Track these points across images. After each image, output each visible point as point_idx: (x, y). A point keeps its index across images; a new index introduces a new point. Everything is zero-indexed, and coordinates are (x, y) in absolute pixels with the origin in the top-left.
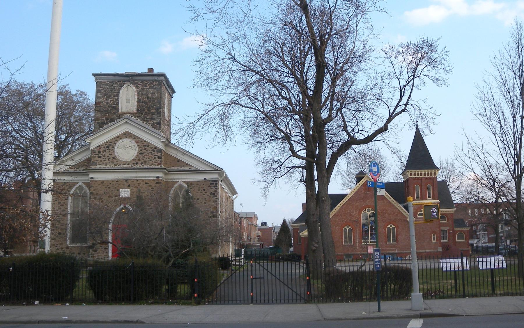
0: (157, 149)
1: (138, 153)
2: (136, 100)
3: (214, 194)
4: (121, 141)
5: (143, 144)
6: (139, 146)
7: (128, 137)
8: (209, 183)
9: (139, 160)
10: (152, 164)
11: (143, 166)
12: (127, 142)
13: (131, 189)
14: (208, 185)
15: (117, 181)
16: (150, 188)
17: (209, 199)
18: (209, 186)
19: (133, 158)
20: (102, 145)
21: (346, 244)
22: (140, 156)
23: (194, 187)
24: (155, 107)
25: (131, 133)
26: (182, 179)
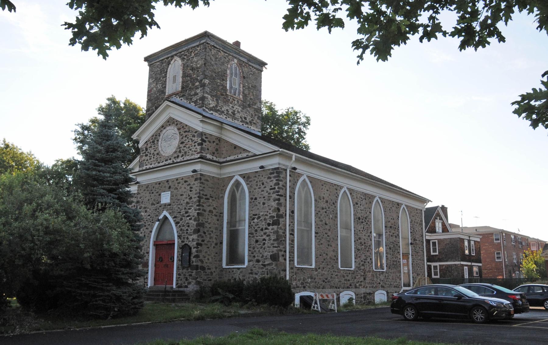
0: (198, 132)
1: (179, 143)
2: (181, 75)
3: (274, 188)
4: (164, 131)
5: (184, 130)
6: (181, 134)
7: (171, 124)
8: (269, 172)
9: (180, 152)
10: (192, 155)
11: (184, 158)
12: (172, 130)
13: (171, 192)
14: (267, 176)
15: (159, 184)
16: (188, 188)
17: (269, 197)
18: (269, 178)
19: (174, 150)
20: (149, 140)
21: (314, 309)
22: (181, 145)
23: (251, 181)
24: (198, 78)
25: (174, 119)
26: (237, 171)
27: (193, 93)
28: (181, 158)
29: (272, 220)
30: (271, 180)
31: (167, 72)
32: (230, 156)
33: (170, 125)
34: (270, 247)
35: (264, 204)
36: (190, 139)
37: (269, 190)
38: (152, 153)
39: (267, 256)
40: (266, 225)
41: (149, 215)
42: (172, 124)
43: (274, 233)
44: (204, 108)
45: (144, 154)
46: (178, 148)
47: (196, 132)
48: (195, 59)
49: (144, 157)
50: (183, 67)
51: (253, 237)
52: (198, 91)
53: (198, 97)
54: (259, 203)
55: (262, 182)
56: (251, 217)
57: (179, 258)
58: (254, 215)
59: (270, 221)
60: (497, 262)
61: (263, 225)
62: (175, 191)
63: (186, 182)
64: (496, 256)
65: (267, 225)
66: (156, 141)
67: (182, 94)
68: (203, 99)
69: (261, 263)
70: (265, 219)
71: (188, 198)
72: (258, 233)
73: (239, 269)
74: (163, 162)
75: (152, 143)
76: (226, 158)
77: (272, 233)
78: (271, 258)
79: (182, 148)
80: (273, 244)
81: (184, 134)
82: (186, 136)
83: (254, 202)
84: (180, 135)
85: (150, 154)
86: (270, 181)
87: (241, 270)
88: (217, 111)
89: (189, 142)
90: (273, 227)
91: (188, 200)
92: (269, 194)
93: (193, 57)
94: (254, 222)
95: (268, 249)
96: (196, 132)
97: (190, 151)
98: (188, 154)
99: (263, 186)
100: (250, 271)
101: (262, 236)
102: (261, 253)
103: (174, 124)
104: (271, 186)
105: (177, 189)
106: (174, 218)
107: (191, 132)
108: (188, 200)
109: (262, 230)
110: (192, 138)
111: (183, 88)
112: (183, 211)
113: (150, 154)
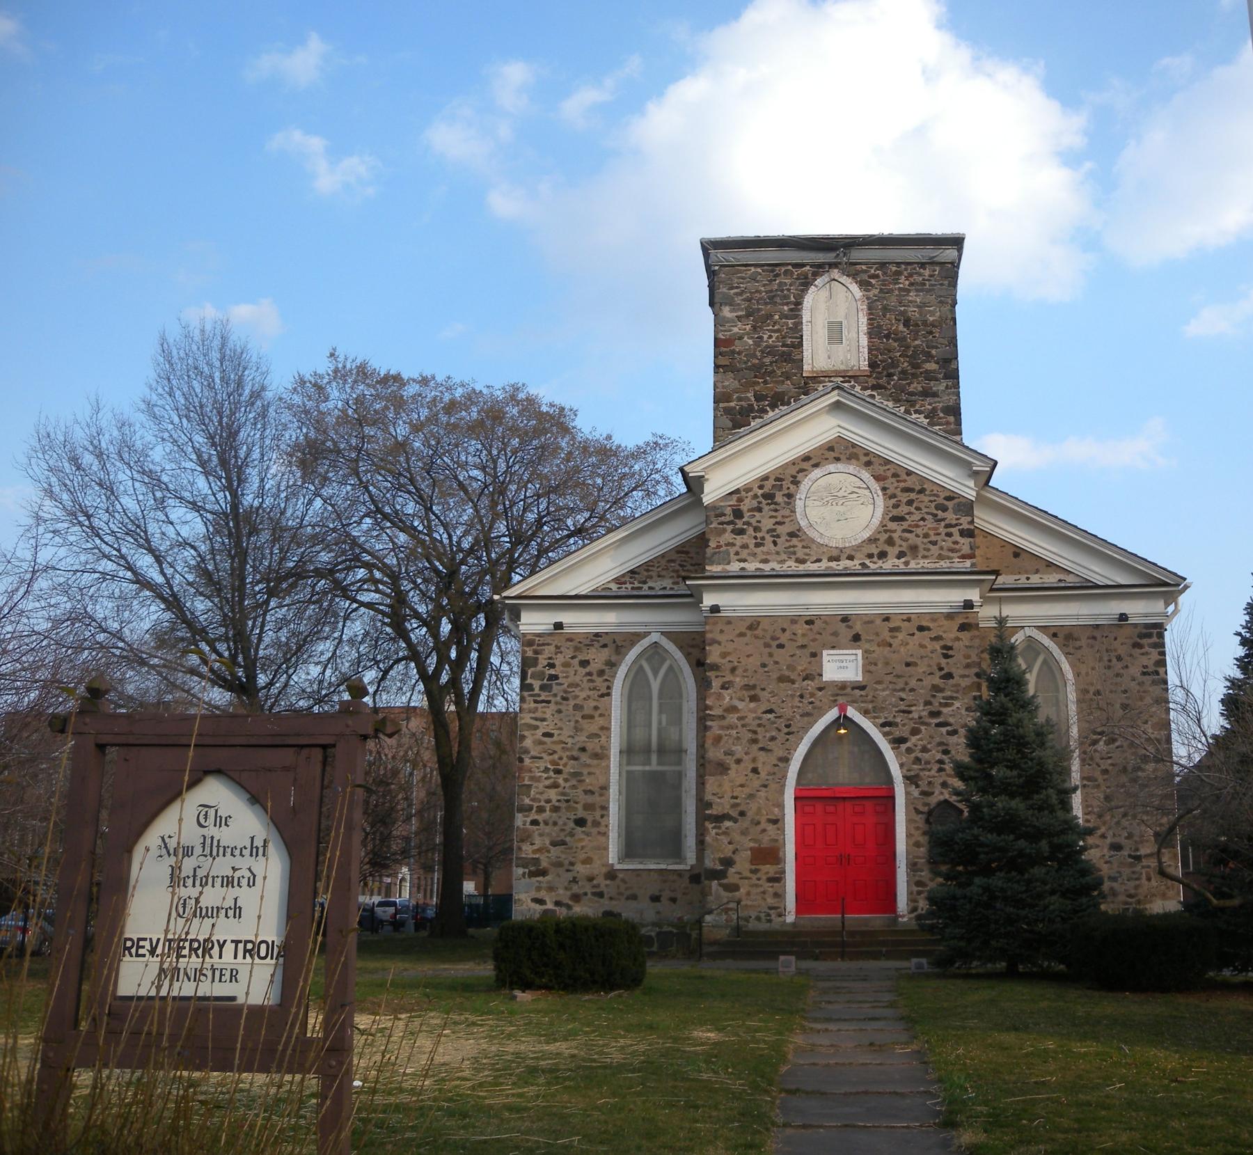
0: (956, 501)
1: (883, 518)
4: (817, 473)
5: (902, 485)
10: (941, 557)
11: (907, 563)
13: (866, 652)
20: (748, 489)
24: (934, 352)
27: (916, 386)
33: (838, 459)
36: (928, 513)
38: (764, 529)
41: (770, 711)
42: (849, 459)
45: (730, 528)
47: (949, 499)
49: (728, 537)
50: (870, 308)
53: (941, 405)
57: (914, 840)
62: (880, 652)
63: (921, 629)
67: (872, 381)
69: (1125, 853)
71: (939, 674)
74: (819, 560)
75: (761, 499)
81: (904, 497)
82: (910, 503)
84: (884, 495)
85: (756, 529)
86: (1143, 654)
91: (937, 680)
93: (908, 291)
96: (949, 499)
97: (931, 547)
98: (922, 552)
102: (1124, 828)
103: (858, 459)
104: (1145, 667)
106: (883, 725)
107: (930, 495)
108: (937, 680)
110: (935, 512)
111: (872, 365)
112: (921, 708)
113: (756, 529)
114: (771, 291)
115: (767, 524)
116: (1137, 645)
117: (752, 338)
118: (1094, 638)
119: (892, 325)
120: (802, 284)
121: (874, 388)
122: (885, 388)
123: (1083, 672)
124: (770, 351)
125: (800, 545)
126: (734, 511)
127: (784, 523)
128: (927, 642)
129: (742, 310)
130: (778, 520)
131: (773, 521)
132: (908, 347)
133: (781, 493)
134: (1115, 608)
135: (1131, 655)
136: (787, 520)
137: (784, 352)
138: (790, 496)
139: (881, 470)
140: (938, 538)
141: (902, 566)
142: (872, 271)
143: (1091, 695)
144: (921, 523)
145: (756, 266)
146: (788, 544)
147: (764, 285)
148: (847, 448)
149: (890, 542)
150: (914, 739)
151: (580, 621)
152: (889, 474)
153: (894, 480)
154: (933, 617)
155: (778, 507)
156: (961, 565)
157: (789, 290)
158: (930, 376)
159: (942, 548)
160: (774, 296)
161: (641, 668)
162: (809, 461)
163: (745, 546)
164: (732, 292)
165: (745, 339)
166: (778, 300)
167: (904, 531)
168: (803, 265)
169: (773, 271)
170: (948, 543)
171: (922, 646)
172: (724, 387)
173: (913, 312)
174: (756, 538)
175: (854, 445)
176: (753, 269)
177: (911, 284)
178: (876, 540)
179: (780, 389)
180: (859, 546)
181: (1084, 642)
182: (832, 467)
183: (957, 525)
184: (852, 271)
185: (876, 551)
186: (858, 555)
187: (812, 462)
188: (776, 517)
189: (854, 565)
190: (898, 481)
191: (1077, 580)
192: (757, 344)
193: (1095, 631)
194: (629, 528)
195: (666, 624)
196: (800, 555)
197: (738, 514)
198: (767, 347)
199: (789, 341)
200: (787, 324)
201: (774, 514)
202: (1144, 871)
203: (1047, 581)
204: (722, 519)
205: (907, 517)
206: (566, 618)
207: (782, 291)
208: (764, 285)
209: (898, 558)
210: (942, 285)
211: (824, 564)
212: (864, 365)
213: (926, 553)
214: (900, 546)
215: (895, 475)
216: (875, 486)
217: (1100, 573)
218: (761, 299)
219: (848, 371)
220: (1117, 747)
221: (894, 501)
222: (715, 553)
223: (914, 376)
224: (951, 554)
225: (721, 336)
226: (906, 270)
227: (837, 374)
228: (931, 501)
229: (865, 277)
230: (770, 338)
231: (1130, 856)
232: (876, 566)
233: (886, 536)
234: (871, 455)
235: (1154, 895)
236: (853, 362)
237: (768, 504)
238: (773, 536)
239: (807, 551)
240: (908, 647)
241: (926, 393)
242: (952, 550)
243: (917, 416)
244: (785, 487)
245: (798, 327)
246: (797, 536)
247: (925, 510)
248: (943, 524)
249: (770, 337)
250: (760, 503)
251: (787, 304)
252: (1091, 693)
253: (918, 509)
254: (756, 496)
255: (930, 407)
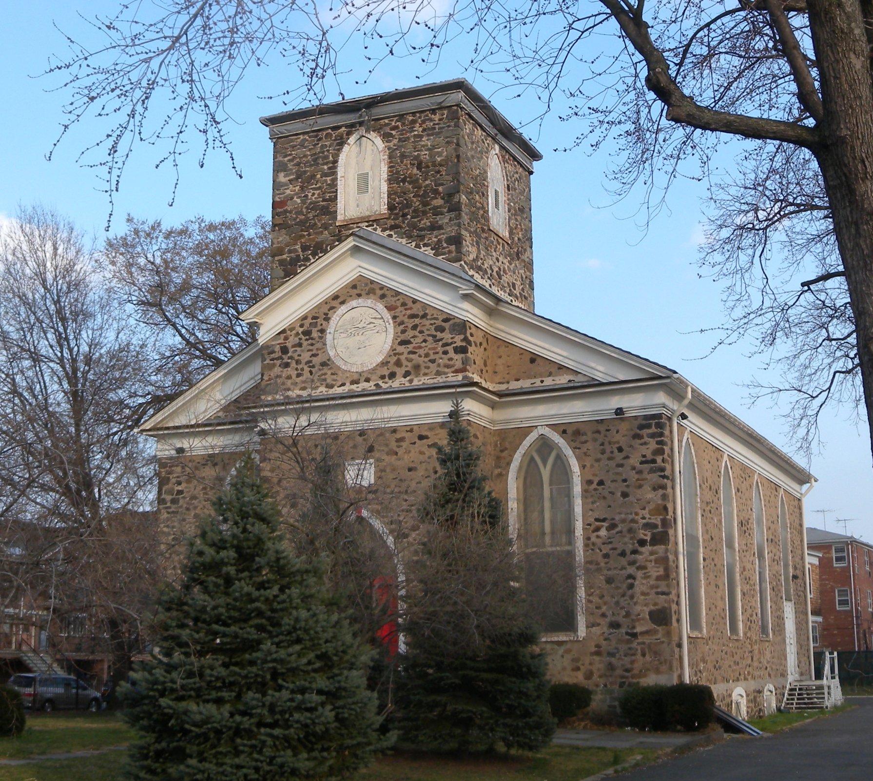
0: (451, 322)
1: (393, 343)
4: (343, 309)
5: (409, 312)
9: (398, 364)
10: (438, 373)
11: (411, 381)
19: (380, 359)
20: (292, 329)
22: (400, 349)
24: (441, 189)
27: (426, 222)
28: (405, 381)
29: (649, 534)
30: (643, 441)
31: (335, 162)
32: (517, 380)
33: (359, 295)
34: (648, 594)
35: (625, 495)
36: (429, 335)
37: (638, 465)
38: (303, 362)
39: (639, 615)
40: (633, 544)
42: (368, 294)
43: (656, 561)
44: (462, 263)
45: (278, 362)
46: (392, 353)
47: (446, 320)
48: (426, 141)
49: (277, 370)
50: (390, 157)
51: (599, 570)
52: (444, 220)
54: (612, 493)
55: (617, 446)
56: (589, 525)
58: (597, 520)
59: (645, 535)
60: (839, 611)
61: (625, 544)
63: (421, 438)
64: (837, 598)
65: (637, 545)
66: (314, 330)
67: (391, 222)
68: (457, 241)
69: (623, 630)
70: (630, 530)
72: (611, 562)
73: (560, 643)
74: (343, 385)
75: (301, 336)
76: (508, 383)
77: (651, 561)
78: (651, 618)
79: (405, 355)
80: (657, 587)
81: (410, 323)
82: (415, 327)
83: (595, 489)
84: (395, 322)
85: (298, 362)
86: (642, 444)
87: (568, 646)
88: (479, 269)
89: (425, 341)
90: (655, 548)
92: (640, 472)
93: (421, 137)
94: (598, 537)
95: (642, 597)
97: (430, 364)
98: (423, 370)
99: (622, 455)
100: (594, 649)
101: (623, 568)
103: (375, 294)
104: (644, 456)
105: (396, 454)
107: (431, 319)
109: (623, 554)
110: (435, 333)
111: (391, 207)
113: (298, 362)
114: (315, 154)
115: (306, 357)
116: (637, 436)
117: (299, 197)
118: (598, 432)
119: (408, 169)
120: (338, 144)
121: (392, 228)
122: (401, 227)
123: (588, 465)
124: (314, 206)
125: (329, 372)
126: (282, 348)
127: (318, 355)
128: (425, 449)
129: (293, 174)
130: (314, 352)
131: (310, 353)
132: (419, 188)
133: (316, 329)
134: (616, 402)
135: (631, 446)
136: (319, 352)
137: (323, 206)
138: (322, 331)
139: (391, 300)
140: (437, 356)
141: (407, 384)
142: (393, 124)
143: (594, 486)
144: (424, 344)
145: (304, 133)
146: (321, 373)
147: (310, 150)
148: (366, 285)
149: (398, 364)
150: (414, 535)
151: (198, 446)
152: (399, 304)
153: (402, 309)
154: (431, 427)
155: (313, 342)
156: (454, 379)
157: (328, 151)
158: (436, 212)
159: (439, 365)
160: (316, 159)
161: (532, 459)
162: (337, 299)
163: (289, 377)
164: (286, 159)
165: (295, 199)
166: (320, 161)
167: (410, 353)
168: (338, 127)
169: (316, 136)
170: (444, 361)
171: (422, 453)
172: (278, 243)
173: (425, 155)
174: (297, 369)
175: (372, 282)
176: (302, 137)
177: (424, 130)
178: (388, 362)
179: (320, 238)
180: (374, 370)
181: (589, 436)
182: (354, 303)
183: (452, 343)
184: (376, 126)
185: (387, 373)
186: (373, 377)
187: (340, 300)
188: (311, 350)
189: (370, 386)
190: (406, 309)
191: (586, 379)
192: (303, 202)
193: (599, 426)
194: (227, 367)
195: (552, 416)
196: (329, 381)
197: (284, 350)
198: (311, 203)
199: (327, 196)
200: (326, 181)
201: (311, 348)
202: (639, 648)
203: (558, 382)
204: (273, 356)
205: (412, 340)
206: (185, 444)
207: (323, 152)
208: (310, 150)
209: (405, 377)
210: (449, 126)
211: (346, 388)
212: (384, 209)
213: (427, 371)
214: (406, 366)
215: (404, 304)
216: (387, 315)
217: (601, 371)
218: (308, 162)
219: (370, 216)
220: (617, 533)
221: (402, 327)
222: (268, 385)
223: (424, 213)
224: (446, 370)
225: (277, 199)
226: (420, 117)
227: (363, 219)
228: (431, 324)
229: (387, 130)
230: (313, 195)
231: (627, 633)
232: (387, 385)
233: (396, 358)
234: (385, 289)
235: (648, 670)
236: (376, 208)
237: (307, 340)
238: (310, 367)
239: (335, 377)
240: (410, 455)
241: (434, 227)
242: (448, 366)
243: (426, 248)
244: (319, 324)
245: (333, 185)
246: (328, 365)
247: (427, 333)
248: (440, 343)
249: (314, 194)
250: (300, 339)
251: (326, 164)
252: (595, 483)
253: (421, 332)
254: (298, 334)
255: (436, 240)
